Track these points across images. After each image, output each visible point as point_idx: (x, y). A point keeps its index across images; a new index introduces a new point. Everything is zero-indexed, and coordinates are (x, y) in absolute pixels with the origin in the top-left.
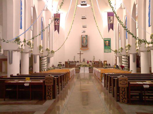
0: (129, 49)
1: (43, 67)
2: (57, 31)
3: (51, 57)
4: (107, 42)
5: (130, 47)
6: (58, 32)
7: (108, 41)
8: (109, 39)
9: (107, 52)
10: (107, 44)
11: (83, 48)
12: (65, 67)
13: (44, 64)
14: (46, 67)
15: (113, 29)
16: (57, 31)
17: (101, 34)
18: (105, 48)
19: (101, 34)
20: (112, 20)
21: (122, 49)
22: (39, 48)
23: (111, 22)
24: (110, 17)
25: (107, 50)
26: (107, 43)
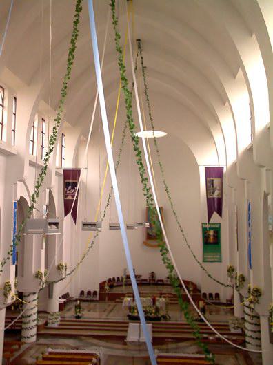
0: (258, 302)
1: (25, 323)
2: (69, 215)
3: (55, 282)
4: (211, 233)
5: (260, 295)
6: (74, 216)
7: (214, 232)
8: (217, 226)
9: (210, 260)
10: (211, 239)
11: (151, 242)
12: (98, 299)
13: (29, 316)
14: (35, 323)
15: (220, 213)
16: (69, 215)
17: (183, 235)
18: (205, 251)
19: (183, 235)
20: (218, 188)
21: (244, 280)
22: (3, 291)
23: (217, 193)
24: (213, 181)
25: (210, 256)
26: (212, 238)
